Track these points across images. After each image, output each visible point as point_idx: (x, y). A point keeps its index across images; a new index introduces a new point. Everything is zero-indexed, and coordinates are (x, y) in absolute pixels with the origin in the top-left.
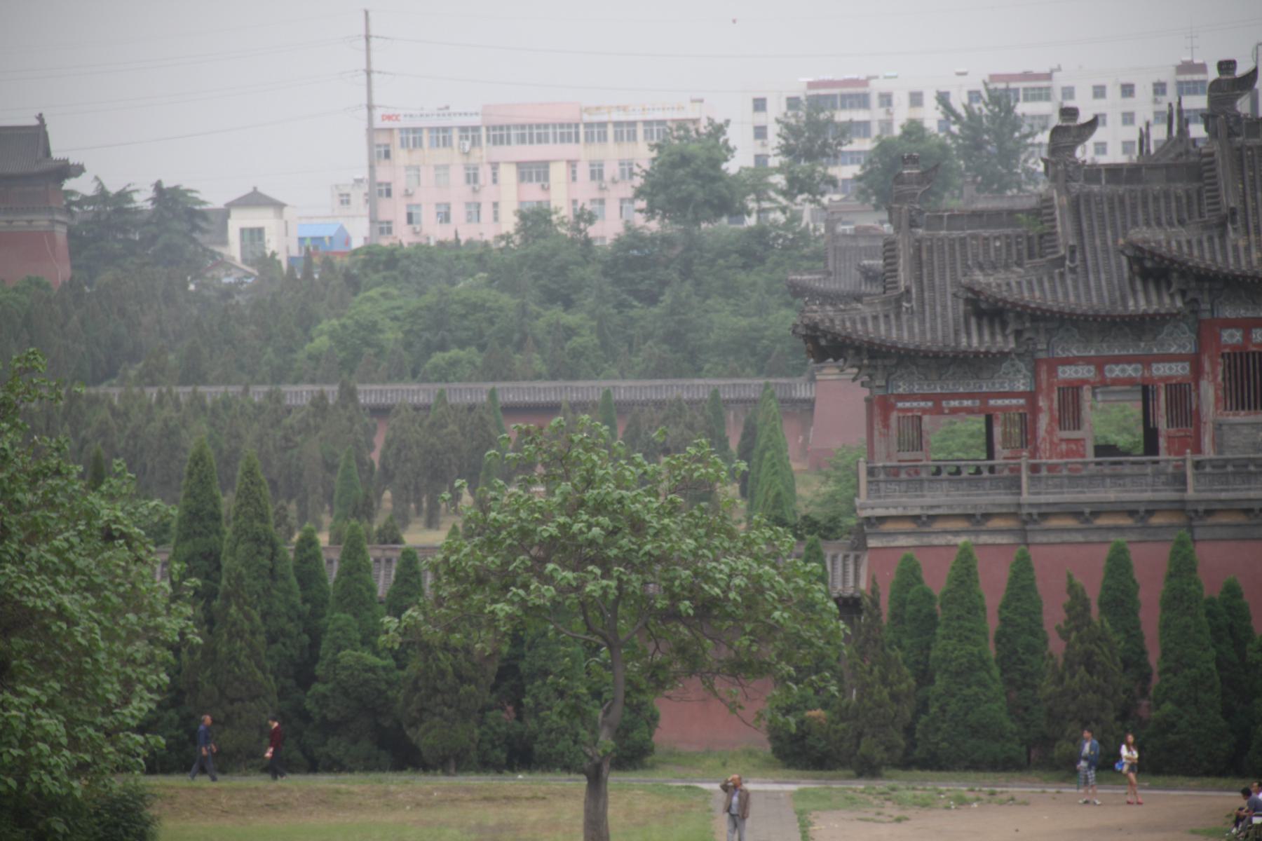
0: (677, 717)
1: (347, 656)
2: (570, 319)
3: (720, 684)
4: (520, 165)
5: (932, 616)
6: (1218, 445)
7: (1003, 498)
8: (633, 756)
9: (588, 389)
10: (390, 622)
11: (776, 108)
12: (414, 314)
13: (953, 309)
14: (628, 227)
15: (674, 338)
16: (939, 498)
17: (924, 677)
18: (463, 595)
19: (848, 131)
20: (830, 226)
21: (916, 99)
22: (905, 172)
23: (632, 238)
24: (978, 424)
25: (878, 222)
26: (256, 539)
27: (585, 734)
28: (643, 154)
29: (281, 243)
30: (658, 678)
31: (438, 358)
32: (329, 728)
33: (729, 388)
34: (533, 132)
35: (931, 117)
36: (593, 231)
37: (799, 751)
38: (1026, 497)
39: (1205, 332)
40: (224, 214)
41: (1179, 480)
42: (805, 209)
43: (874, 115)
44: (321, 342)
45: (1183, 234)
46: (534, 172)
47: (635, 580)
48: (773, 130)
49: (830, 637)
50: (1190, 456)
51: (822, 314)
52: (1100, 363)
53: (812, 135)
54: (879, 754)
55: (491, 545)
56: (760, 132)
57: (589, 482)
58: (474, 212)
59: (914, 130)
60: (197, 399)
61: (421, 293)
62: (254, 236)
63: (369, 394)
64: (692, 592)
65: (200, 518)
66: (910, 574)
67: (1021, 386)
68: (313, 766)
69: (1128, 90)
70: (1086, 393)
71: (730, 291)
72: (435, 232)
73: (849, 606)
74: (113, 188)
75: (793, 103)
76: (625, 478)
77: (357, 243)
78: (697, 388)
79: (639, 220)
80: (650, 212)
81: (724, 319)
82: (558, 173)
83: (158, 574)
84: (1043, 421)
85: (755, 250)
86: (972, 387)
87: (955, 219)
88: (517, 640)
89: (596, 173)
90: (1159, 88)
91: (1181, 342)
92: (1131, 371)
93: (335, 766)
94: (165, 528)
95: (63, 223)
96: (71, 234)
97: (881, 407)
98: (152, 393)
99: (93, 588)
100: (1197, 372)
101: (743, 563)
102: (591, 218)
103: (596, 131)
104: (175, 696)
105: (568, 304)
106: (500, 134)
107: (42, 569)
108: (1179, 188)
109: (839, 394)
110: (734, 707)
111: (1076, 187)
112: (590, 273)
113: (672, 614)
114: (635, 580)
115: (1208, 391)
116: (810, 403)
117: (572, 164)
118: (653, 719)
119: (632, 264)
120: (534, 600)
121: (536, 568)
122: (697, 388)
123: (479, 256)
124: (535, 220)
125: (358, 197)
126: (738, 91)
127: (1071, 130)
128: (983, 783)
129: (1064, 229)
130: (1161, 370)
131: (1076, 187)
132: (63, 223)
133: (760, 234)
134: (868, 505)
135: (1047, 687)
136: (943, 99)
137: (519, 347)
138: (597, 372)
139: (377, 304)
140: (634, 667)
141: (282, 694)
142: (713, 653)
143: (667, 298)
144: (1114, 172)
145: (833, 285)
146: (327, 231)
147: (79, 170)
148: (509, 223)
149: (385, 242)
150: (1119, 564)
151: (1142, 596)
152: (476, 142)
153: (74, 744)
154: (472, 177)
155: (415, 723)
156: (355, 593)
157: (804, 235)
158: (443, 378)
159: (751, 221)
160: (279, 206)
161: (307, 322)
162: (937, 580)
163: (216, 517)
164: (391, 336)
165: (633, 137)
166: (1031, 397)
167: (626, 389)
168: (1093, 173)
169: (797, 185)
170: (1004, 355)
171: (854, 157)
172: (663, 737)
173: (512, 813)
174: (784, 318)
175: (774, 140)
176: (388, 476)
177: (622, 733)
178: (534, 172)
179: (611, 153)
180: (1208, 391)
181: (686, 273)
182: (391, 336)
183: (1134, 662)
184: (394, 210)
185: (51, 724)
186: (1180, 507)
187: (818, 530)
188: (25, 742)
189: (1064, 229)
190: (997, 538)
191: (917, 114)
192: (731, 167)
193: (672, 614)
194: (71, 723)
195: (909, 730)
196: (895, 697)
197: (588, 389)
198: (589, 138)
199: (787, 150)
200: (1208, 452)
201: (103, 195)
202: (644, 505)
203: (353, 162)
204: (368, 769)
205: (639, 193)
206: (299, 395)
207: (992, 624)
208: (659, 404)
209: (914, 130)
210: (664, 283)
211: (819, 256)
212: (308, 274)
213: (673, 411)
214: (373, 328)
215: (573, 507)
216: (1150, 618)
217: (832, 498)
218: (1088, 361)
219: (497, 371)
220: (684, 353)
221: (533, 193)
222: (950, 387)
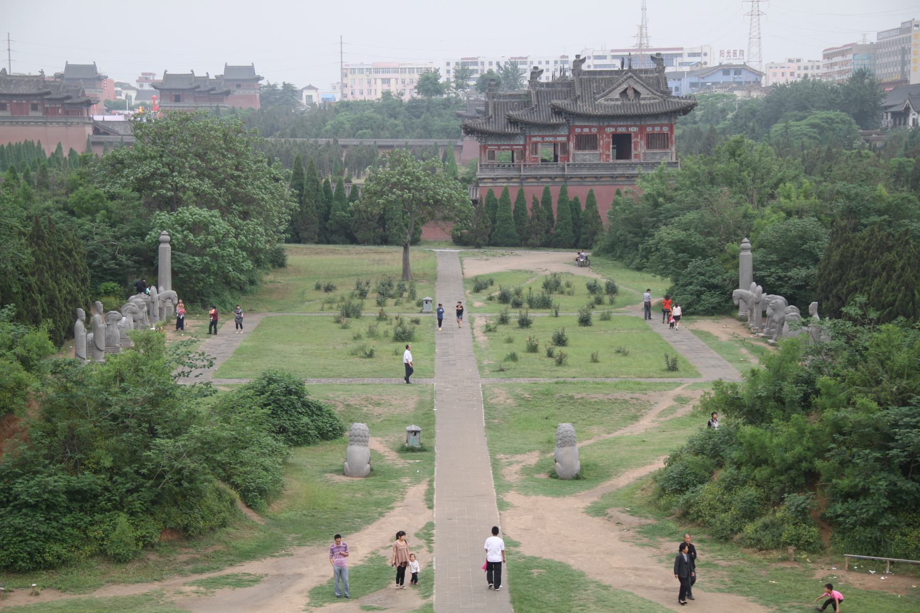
0: (426, 232)
1: (338, 213)
2: (396, 122)
3: (440, 223)
4: (383, 79)
5: (497, 205)
6: (574, 160)
7: (516, 173)
8: (415, 242)
9: (401, 141)
10: (351, 204)
11: (453, 65)
12: (353, 120)
13: (503, 121)
14: (412, 97)
15: (425, 128)
16: (499, 173)
17: (494, 221)
18: (370, 198)
19: (473, 71)
20: (468, 98)
21: (491, 63)
22: (489, 83)
23: (413, 100)
24: (510, 152)
25: (482, 97)
26: (313, 180)
27: (402, 236)
28: (416, 77)
29: (317, 99)
30: (423, 221)
31: (360, 132)
32: (333, 232)
33: (439, 142)
34: (386, 70)
35: (495, 68)
36: (403, 98)
37: (460, 241)
38: (522, 173)
39: (571, 129)
40: (302, 91)
41: (563, 169)
42: (460, 92)
43: (479, 67)
44: (328, 127)
45: (566, 102)
46: (386, 81)
47: (417, 194)
48: (452, 71)
49: (470, 210)
50: (566, 163)
51: (468, 122)
52: (543, 137)
53: (463, 73)
54: (482, 242)
55: (378, 184)
56: (448, 72)
57: (405, 167)
58: (370, 92)
59: (490, 72)
60: (295, 141)
61: (356, 114)
62: (310, 97)
63: (341, 142)
64: (433, 198)
65: (298, 174)
66: (491, 193)
67: (522, 143)
68: (328, 243)
69: (547, 62)
70: (539, 146)
71: (440, 115)
72: (359, 97)
73: (475, 202)
74: (272, 84)
75: (457, 64)
76: (417, 168)
77: (338, 100)
78: (431, 142)
79: (415, 95)
80: (418, 93)
81: (438, 123)
82: (393, 82)
83: (287, 190)
84: (527, 153)
85: (447, 104)
86: (508, 143)
87: (505, 96)
88: (385, 210)
89: (403, 82)
90: (556, 62)
91: (564, 131)
92: (551, 139)
93: (334, 243)
94: (289, 177)
95: (644, 99)
96: (260, 96)
97: (484, 148)
98: (283, 140)
99: (272, 193)
100: (569, 140)
101: (447, 190)
102: (402, 95)
103: (403, 70)
104: (292, 223)
105: (396, 118)
106: (377, 71)
107: (258, 187)
108: (565, 89)
109: (471, 145)
110: (443, 229)
111: (537, 88)
112: (402, 109)
113: (428, 204)
114: (417, 194)
115: (572, 145)
116: (462, 146)
117: (397, 79)
118: (420, 232)
119: (414, 108)
120: (390, 199)
121: (391, 191)
122: (431, 142)
123: (371, 104)
124: (387, 94)
125: (338, 88)
126: (442, 60)
127: (536, 73)
128: (509, 250)
129: (534, 99)
130: (559, 139)
131: (537, 88)
132: (644, 99)
133: (448, 99)
134: (479, 174)
135: (527, 225)
136: (498, 64)
137: (382, 129)
138: (404, 137)
139: (343, 117)
140: (416, 218)
141: (320, 223)
142: (438, 215)
143: (423, 117)
144: (548, 84)
145: (469, 114)
146: (329, 96)
147: (263, 78)
148: (379, 96)
149: (346, 100)
150: (547, 192)
151: (553, 200)
152: (370, 73)
153: (267, 235)
154: (369, 82)
155: (356, 232)
156: (340, 195)
157: (460, 100)
158: (362, 138)
159: (445, 96)
160: (317, 89)
161: (324, 121)
162: (498, 195)
163: (302, 174)
164: (347, 126)
165: (413, 72)
166: (524, 146)
167: (411, 142)
168: (542, 85)
169: (459, 86)
170: (517, 134)
171: (474, 79)
172: (423, 237)
173: (382, 256)
174: (456, 124)
175: (452, 74)
176: (346, 164)
177: (413, 235)
178: (386, 81)
179: (407, 76)
180: (572, 145)
181: (428, 110)
182: (347, 126)
183: (550, 218)
184: (348, 91)
185: (261, 229)
186: (563, 176)
187: (466, 181)
188: (254, 234)
189: (534, 99)
190: (514, 184)
191: (491, 67)
192: (441, 81)
193: (428, 204)
194: (266, 230)
195: (490, 236)
196: (486, 227)
197: (401, 141)
198: (401, 72)
199: (456, 77)
200: (571, 162)
201: (269, 85)
202: (420, 173)
203: (337, 78)
204: (343, 243)
205: (415, 88)
206: (322, 141)
207: (513, 207)
208: (420, 146)
209: (490, 72)
210: (422, 113)
211: (464, 106)
212: (324, 108)
213: (425, 148)
214: (343, 123)
215: (401, 174)
216: (554, 206)
217: (468, 173)
218: (540, 136)
219: (376, 136)
220: (428, 132)
221: (386, 87)
222: (503, 143)
